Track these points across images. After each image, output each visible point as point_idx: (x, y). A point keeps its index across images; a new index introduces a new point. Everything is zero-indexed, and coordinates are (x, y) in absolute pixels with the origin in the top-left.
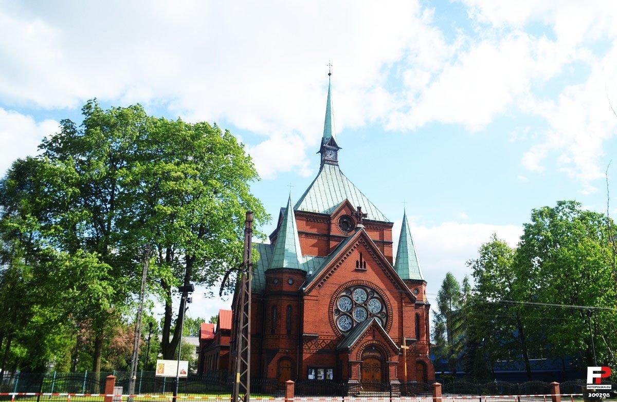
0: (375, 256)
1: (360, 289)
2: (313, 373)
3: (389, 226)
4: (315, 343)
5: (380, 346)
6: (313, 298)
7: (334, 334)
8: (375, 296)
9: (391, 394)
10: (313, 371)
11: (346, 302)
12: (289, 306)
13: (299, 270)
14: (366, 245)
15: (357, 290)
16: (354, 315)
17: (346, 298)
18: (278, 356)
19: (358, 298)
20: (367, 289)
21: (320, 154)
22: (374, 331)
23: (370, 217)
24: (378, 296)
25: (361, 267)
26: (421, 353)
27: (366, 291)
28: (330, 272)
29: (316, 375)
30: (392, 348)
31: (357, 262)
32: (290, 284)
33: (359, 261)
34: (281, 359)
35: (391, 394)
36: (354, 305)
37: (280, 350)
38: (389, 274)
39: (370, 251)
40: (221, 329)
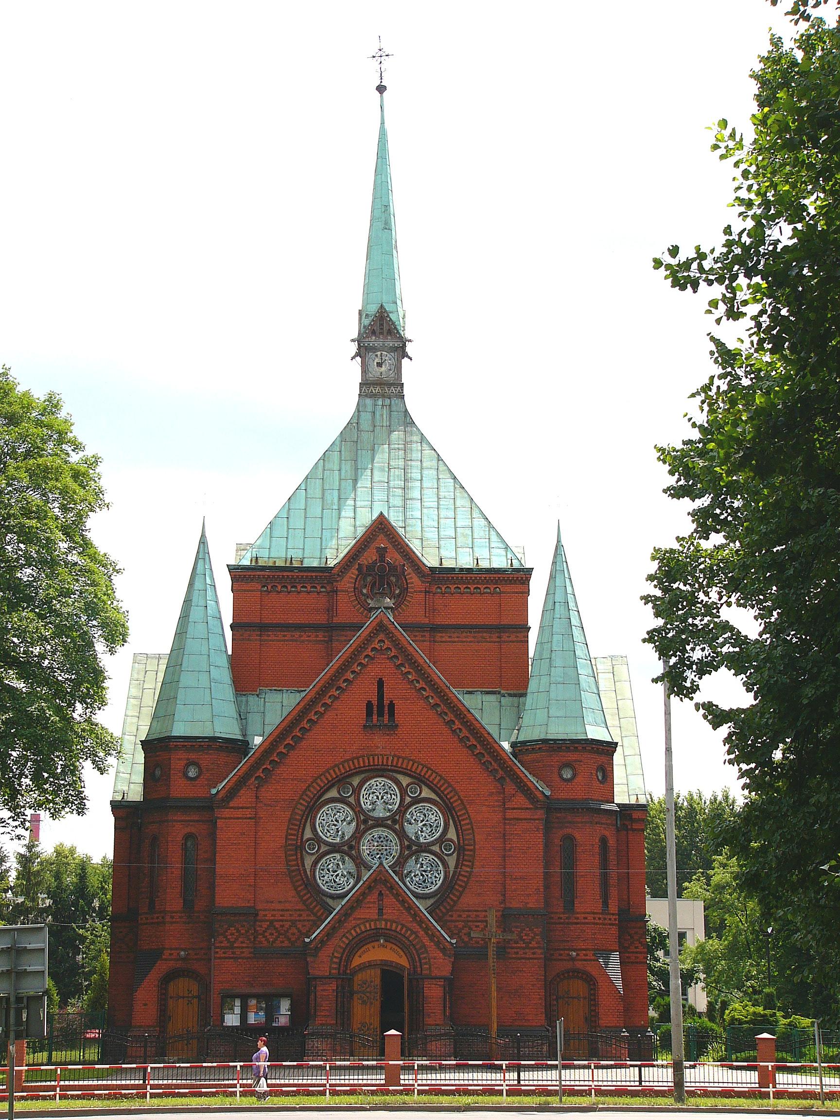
0: (422, 684)
1: (380, 779)
2: (237, 1010)
3: (520, 577)
4: (247, 931)
5: (407, 938)
6: (239, 813)
7: (300, 906)
8: (423, 795)
9: (822, 1088)
10: (238, 1003)
11: (340, 816)
12: (188, 836)
13: (214, 739)
14: (396, 657)
15: (372, 781)
16: (365, 848)
17: (340, 805)
18: (160, 968)
19: (373, 803)
20: (400, 777)
21: (358, 359)
22: (381, 894)
23: (431, 561)
24: (433, 796)
25: (381, 714)
26: (574, 950)
27: (398, 783)
28: (288, 741)
29: (244, 1017)
30: (432, 940)
31: (369, 705)
32: (191, 779)
33: (375, 702)
34: (169, 978)
35: (822, 1088)
36: (366, 822)
37: (167, 953)
38: (465, 733)
39: (409, 673)
40: (626, 809)
